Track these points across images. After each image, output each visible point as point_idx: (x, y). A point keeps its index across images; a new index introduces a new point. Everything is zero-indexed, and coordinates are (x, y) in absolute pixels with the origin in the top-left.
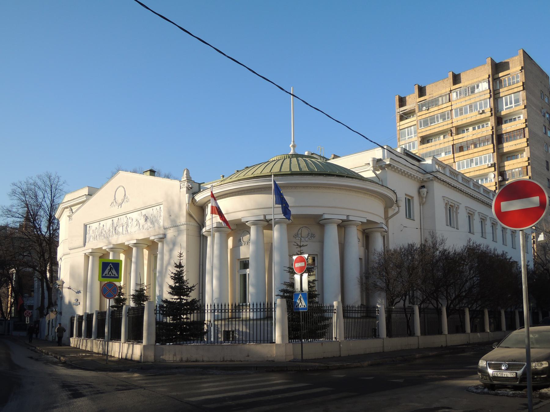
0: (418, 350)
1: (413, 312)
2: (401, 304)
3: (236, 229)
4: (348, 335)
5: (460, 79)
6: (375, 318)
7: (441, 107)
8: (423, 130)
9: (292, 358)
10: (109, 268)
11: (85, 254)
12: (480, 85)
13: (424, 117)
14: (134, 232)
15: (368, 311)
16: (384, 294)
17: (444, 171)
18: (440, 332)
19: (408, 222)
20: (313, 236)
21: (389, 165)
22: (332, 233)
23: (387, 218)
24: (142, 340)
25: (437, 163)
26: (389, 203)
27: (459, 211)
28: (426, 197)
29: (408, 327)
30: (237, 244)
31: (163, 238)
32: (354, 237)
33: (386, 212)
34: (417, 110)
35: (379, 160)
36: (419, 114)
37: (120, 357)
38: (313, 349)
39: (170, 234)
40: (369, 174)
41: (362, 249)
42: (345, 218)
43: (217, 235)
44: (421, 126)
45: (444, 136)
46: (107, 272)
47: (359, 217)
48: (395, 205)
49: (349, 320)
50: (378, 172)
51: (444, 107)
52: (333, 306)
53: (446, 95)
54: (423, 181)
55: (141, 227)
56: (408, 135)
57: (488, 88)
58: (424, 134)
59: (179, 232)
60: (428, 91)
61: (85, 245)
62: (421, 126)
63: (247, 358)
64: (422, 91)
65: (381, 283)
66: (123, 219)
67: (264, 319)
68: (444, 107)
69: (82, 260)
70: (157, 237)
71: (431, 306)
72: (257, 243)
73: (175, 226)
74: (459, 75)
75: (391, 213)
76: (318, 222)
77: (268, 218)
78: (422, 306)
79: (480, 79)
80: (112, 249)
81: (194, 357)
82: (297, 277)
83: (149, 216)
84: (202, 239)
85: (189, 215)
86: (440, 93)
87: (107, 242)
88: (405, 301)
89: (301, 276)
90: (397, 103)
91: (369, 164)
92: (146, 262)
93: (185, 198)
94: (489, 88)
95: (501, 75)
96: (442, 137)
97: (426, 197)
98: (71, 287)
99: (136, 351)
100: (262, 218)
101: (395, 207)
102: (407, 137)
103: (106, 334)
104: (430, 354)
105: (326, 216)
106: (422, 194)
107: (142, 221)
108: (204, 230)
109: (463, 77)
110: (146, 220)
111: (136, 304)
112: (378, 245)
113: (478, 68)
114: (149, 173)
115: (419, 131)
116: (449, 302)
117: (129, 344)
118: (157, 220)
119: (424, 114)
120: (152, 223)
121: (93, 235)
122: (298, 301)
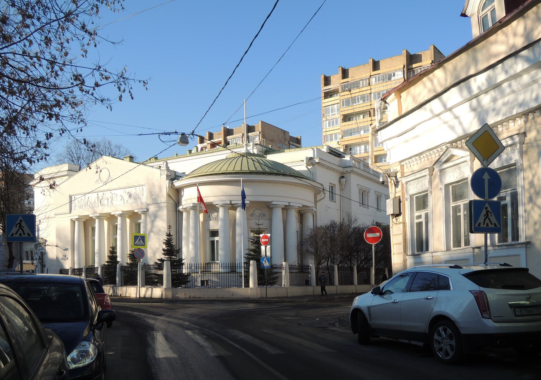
0: (337, 294)
1: (333, 269)
2: (325, 264)
3: (209, 209)
4: (292, 283)
5: (379, 66)
6: (309, 273)
7: (361, 90)
8: (345, 109)
9: (260, 296)
10: (484, 212)
11: (71, 219)
12: (396, 73)
13: (346, 97)
14: (119, 205)
15: (302, 269)
16: (313, 257)
17: (359, 165)
18: (352, 283)
19: (332, 204)
20: (264, 215)
21: (318, 163)
22: (278, 215)
23: (316, 202)
24: (457, 247)
25: (353, 159)
26: (318, 191)
27: (369, 195)
28: (345, 185)
29: (330, 280)
30: (207, 219)
31: (146, 212)
32: (293, 217)
33: (315, 197)
34: (340, 90)
35: (311, 159)
36: (342, 94)
37: (138, 296)
38: (272, 291)
39: (152, 209)
40: (302, 168)
41: (298, 224)
42: (287, 204)
43: (192, 212)
44: (343, 106)
45: (363, 116)
46: (137, 242)
47: (297, 203)
48: (322, 192)
49: (293, 274)
50: (309, 167)
51: (364, 90)
52: (282, 265)
53: (366, 79)
54: (343, 173)
55: (125, 201)
56: (332, 112)
57: (402, 77)
58: (346, 113)
59: (160, 208)
60: (350, 73)
61: (70, 212)
62: (343, 106)
63: (232, 296)
64: (345, 74)
65: (312, 250)
66: (108, 194)
67: (231, 272)
68: (364, 90)
69: (68, 224)
70: (140, 210)
71: (346, 265)
72: (224, 220)
73: (156, 202)
74: (379, 62)
75: (319, 198)
76: (269, 207)
77: (233, 202)
78: (340, 265)
79: (396, 68)
80: (98, 217)
81: (198, 296)
82: (263, 248)
83: (133, 193)
84: (178, 214)
85: (169, 196)
86: (361, 76)
87: (92, 211)
88: (328, 262)
89: (266, 247)
90: (323, 82)
91: (303, 161)
92: (128, 228)
93: (166, 183)
94: (404, 77)
95: (414, 66)
96: (362, 116)
97: (345, 185)
98: (59, 245)
99: (157, 292)
100: (229, 202)
101: (322, 193)
102: (331, 114)
103: (117, 282)
104: (344, 296)
105: (274, 203)
106: (342, 182)
107: (126, 197)
108: (180, 207)
109: (382, 64)
110: (130, 196)
111: (132, 260)
112: (310, 223)
113: (395, 58)
114: (128, 159)
115: (342, 110)
116: (359, 262)
117: (147, 288)
118: (139, 198)
119: (346, 95)
120: (135, 199)
121: (79, 205)
122: (264, 262)
